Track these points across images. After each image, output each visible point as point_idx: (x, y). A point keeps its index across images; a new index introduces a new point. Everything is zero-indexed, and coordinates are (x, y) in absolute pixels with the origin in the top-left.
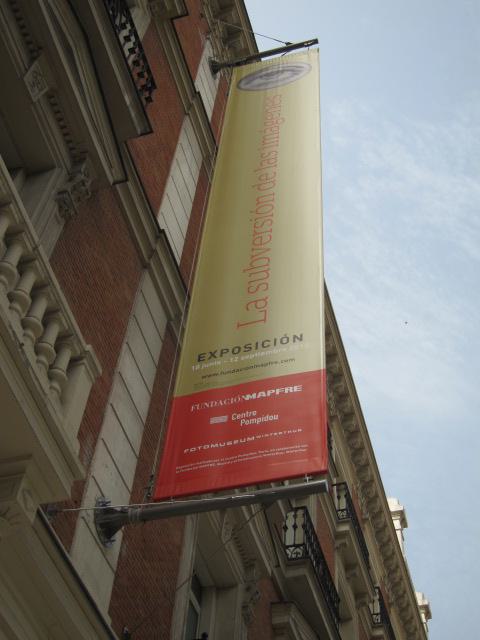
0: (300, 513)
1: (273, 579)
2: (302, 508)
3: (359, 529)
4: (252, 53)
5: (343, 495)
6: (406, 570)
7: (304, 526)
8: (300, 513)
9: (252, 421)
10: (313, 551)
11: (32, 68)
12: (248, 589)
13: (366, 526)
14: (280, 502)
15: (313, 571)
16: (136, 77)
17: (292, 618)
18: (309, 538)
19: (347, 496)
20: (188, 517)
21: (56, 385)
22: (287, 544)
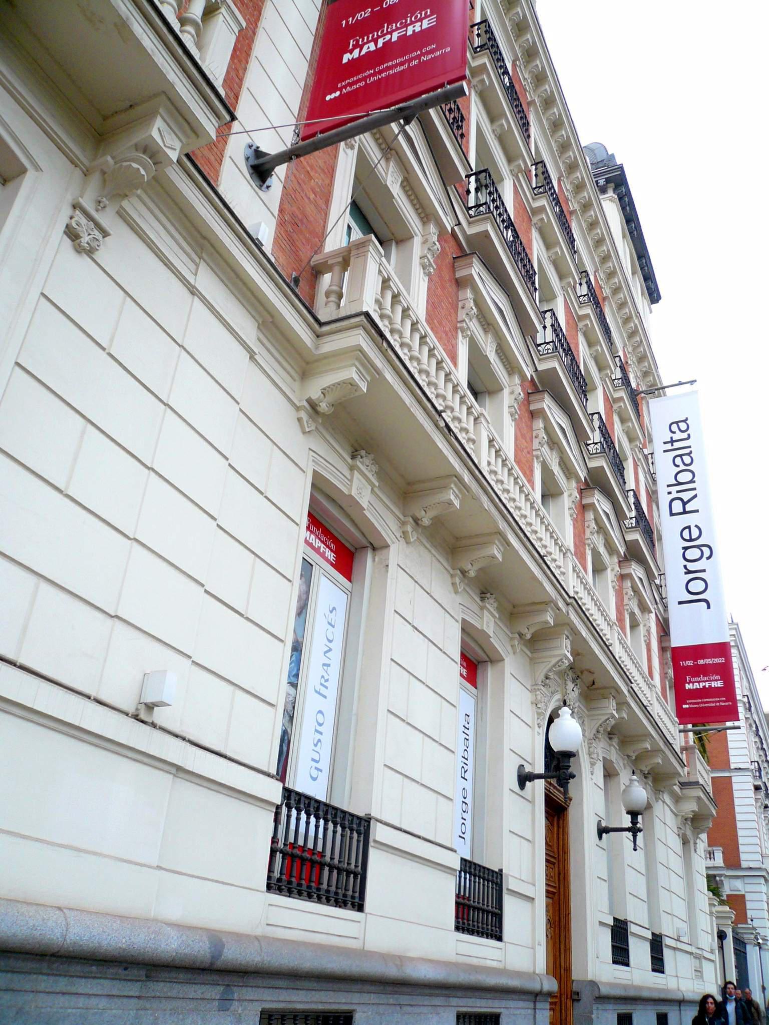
0: (548, 315)
1: (454, 234)
2: (551, 310)
3: (601, 311)
4: (659, 386)
5: (584, 281)
6: (564, 105)
7: (552, 325)
8: (548, 315)
9: (722, 704)
10: (562, 345)
11: (390, 172)
12: (425, 242)
13: (573, 217)
14: (432, 111)
15: (561, 362)
16: (447, 113)
17: (547, 404)
18: (557, 336)
19: (589, 283)
20: (342, 144)
21: (189, 28)
22: (538, 342)
